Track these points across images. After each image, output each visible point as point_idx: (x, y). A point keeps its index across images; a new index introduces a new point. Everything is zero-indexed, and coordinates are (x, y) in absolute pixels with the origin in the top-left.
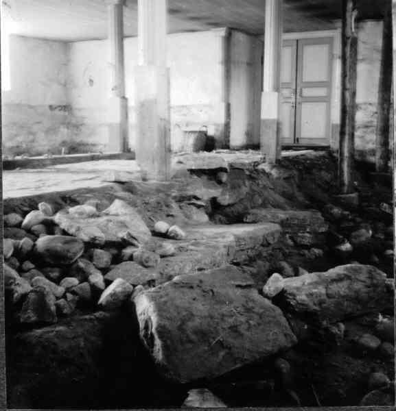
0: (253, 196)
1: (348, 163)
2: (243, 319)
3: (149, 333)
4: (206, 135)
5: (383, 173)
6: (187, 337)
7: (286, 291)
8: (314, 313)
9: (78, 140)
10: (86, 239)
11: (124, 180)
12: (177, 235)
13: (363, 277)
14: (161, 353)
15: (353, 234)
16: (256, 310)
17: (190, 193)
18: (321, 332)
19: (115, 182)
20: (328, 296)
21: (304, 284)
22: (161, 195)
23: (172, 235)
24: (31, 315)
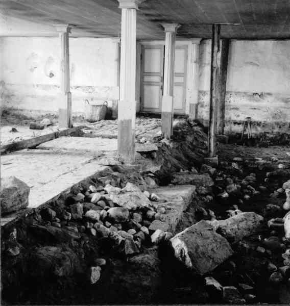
0: (167, 163)
1: (214, 139)
2: (215, 245)
3: (183, 255)
4: (106, 107)
5: (221, 135)
6: (199, 255)
7: (221, 228)
8: (233, 238)
9: (9, 106)
10: (130, 208)
11: (113, 164)
12: (156, 199)
13: (251, 218)
14: (191, 263)
15: (228, 187)
16: (218, 240)
17: (148, 170)
18: (239, 247)
19: (109, 165)
20: (239, 229)
21: (227, 224)
22: (135, 172)
23: (154, 199)
24: (131, 250)
